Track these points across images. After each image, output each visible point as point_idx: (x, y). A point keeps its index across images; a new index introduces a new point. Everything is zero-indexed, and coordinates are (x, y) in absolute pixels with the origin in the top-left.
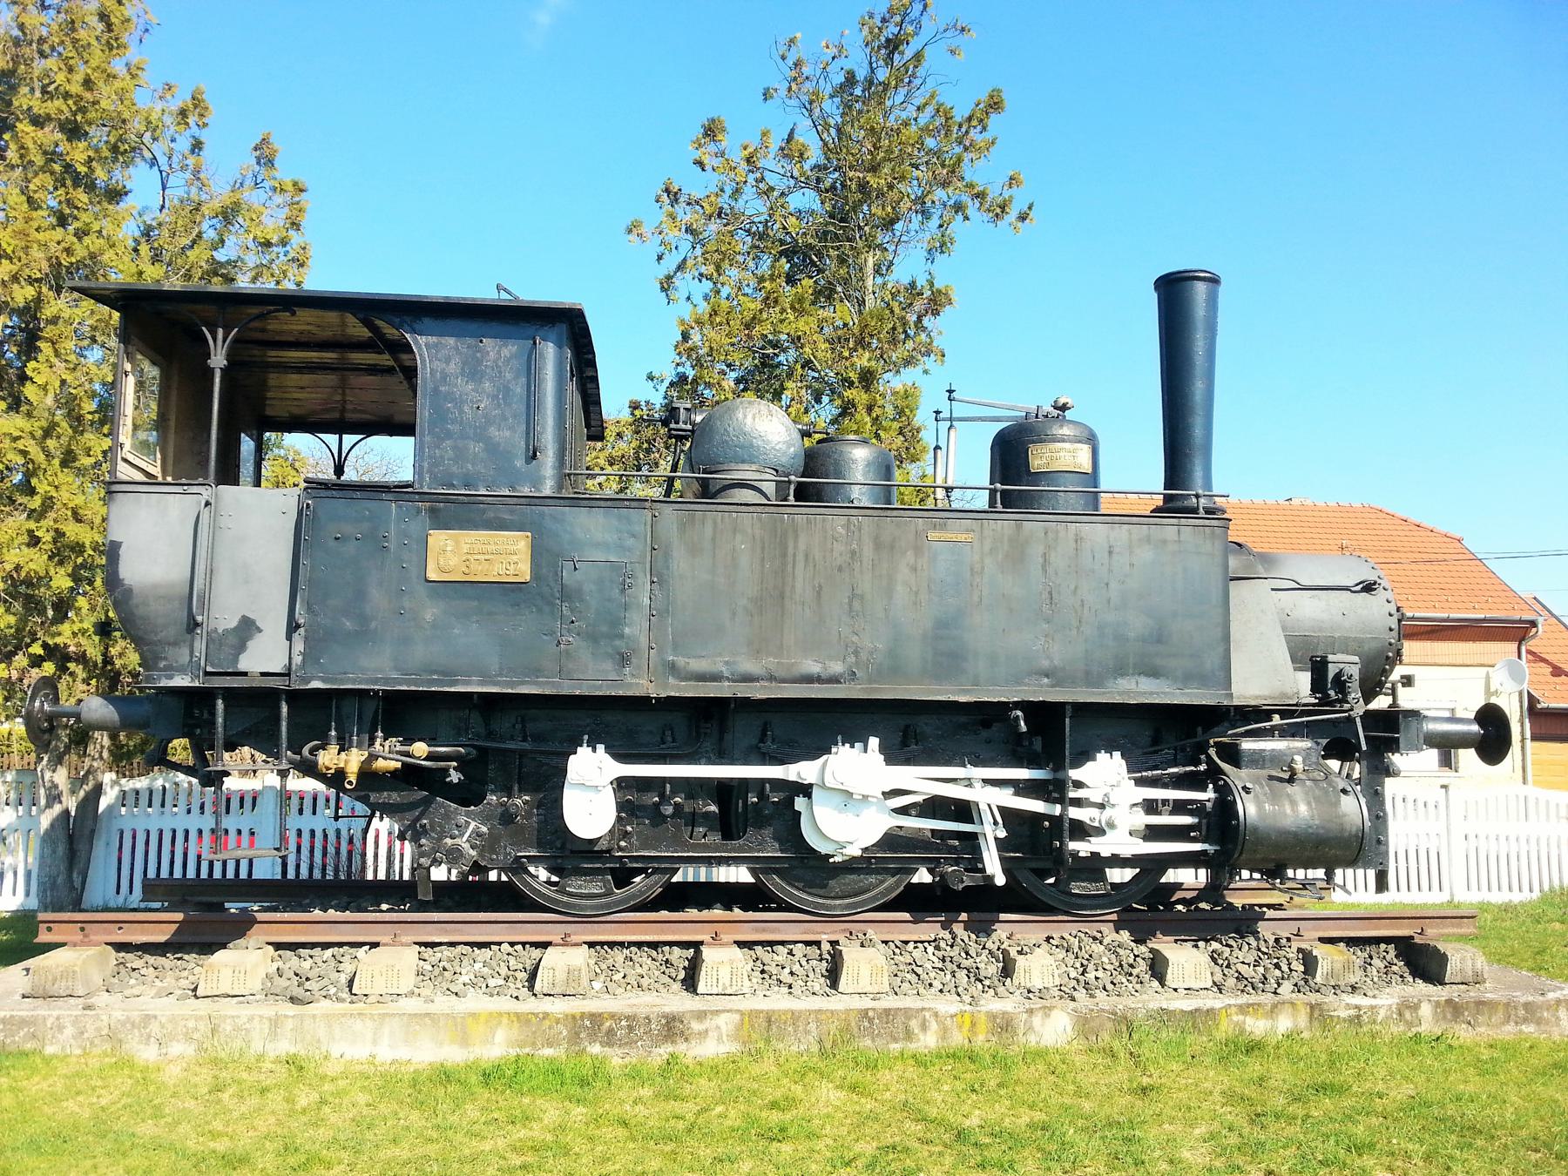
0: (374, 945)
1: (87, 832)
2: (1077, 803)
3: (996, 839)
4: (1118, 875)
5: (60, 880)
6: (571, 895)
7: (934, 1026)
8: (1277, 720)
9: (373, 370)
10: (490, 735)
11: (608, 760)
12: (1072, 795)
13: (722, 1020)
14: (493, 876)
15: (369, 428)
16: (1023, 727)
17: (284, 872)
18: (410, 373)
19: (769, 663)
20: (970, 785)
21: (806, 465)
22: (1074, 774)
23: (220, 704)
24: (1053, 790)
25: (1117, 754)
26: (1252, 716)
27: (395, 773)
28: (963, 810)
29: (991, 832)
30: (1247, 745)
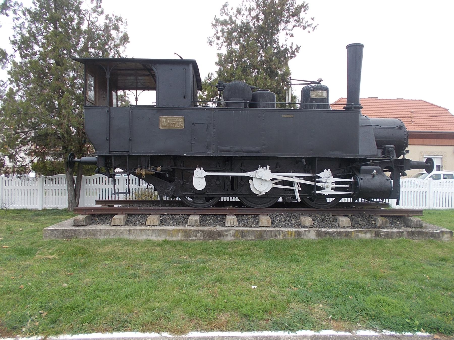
0: (150, 214)
1: (79, 189)
2: (319, 182)
3: (299, 190)
4: (329, 200)
5: (73, 201)
6: (196, 203)
7: (282, 234)
8: (371, 161)
9: (144, 75)
10: (175, 165)
12: (317, 180)
13: (231, 232)
14: (177, 199)
15: (144, 89)
16: (305, 163)
17: (126, 199)
18: (154, 76)
19: (237, 148)
20: (292, 178)
21: (253, 98)
22: (318, 175)
23: (113, 158)
25: (329, 170)
26: (365, 161)
27: (153, 175)
28: (291, 184)
29: (297, 189)
30: (363, 167)
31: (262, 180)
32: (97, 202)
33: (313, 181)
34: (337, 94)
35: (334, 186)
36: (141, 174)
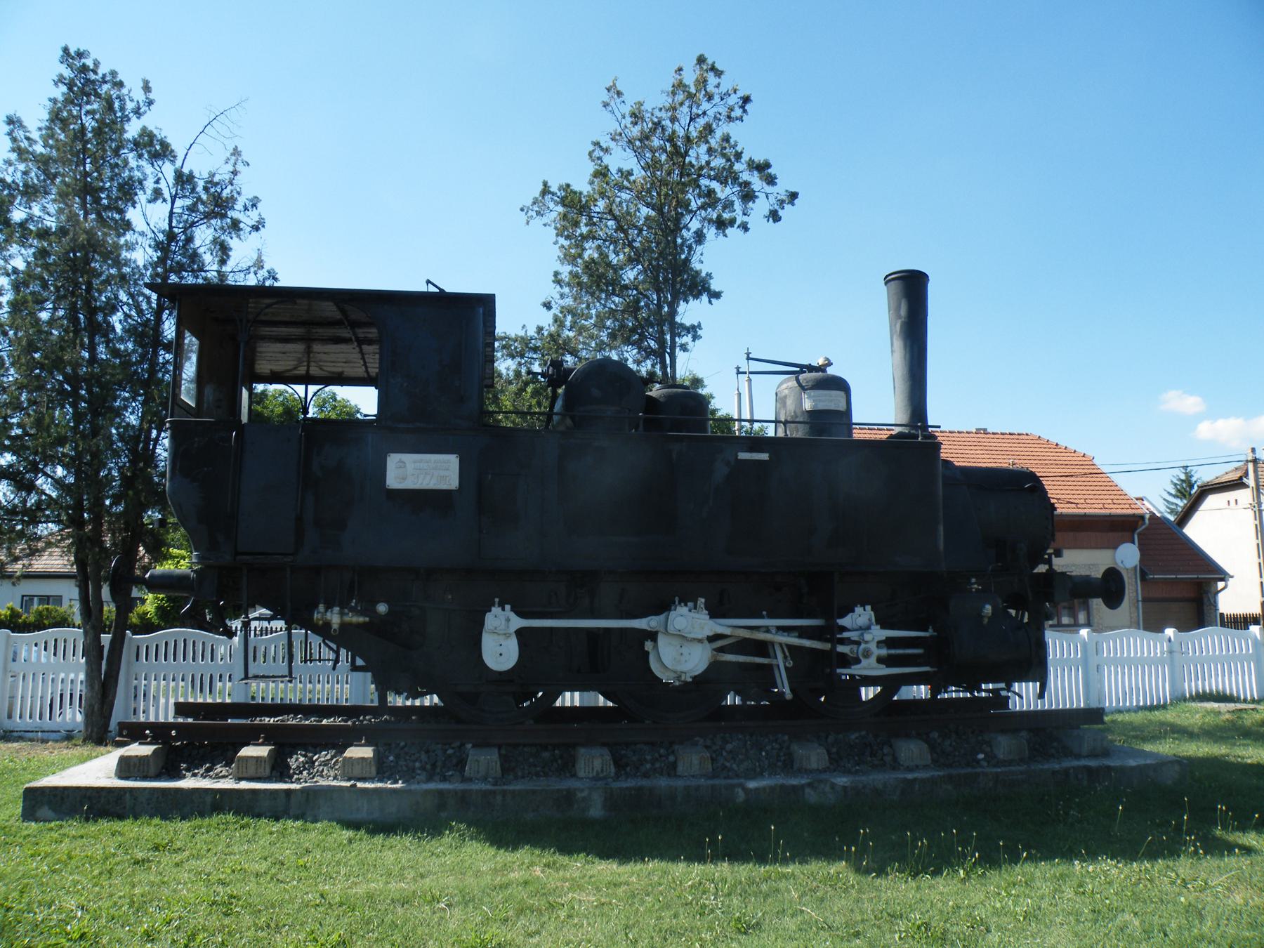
2: (843, 642)
3: (786, 668)
11: (513, 616)
22: (841, 622)
24: (830, 632)
25: (868, 608)
28: (762, 648)
29: (781, 662)
31: (684, 643)
32: (181, 709)
33: (827, 640)
34: (876, 408)
35: (884, 652)
36: (328, 625)
